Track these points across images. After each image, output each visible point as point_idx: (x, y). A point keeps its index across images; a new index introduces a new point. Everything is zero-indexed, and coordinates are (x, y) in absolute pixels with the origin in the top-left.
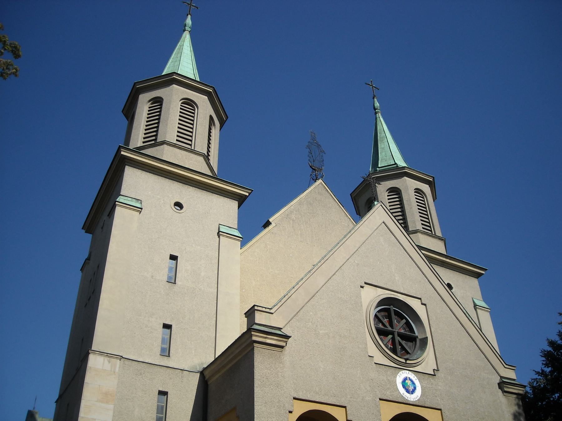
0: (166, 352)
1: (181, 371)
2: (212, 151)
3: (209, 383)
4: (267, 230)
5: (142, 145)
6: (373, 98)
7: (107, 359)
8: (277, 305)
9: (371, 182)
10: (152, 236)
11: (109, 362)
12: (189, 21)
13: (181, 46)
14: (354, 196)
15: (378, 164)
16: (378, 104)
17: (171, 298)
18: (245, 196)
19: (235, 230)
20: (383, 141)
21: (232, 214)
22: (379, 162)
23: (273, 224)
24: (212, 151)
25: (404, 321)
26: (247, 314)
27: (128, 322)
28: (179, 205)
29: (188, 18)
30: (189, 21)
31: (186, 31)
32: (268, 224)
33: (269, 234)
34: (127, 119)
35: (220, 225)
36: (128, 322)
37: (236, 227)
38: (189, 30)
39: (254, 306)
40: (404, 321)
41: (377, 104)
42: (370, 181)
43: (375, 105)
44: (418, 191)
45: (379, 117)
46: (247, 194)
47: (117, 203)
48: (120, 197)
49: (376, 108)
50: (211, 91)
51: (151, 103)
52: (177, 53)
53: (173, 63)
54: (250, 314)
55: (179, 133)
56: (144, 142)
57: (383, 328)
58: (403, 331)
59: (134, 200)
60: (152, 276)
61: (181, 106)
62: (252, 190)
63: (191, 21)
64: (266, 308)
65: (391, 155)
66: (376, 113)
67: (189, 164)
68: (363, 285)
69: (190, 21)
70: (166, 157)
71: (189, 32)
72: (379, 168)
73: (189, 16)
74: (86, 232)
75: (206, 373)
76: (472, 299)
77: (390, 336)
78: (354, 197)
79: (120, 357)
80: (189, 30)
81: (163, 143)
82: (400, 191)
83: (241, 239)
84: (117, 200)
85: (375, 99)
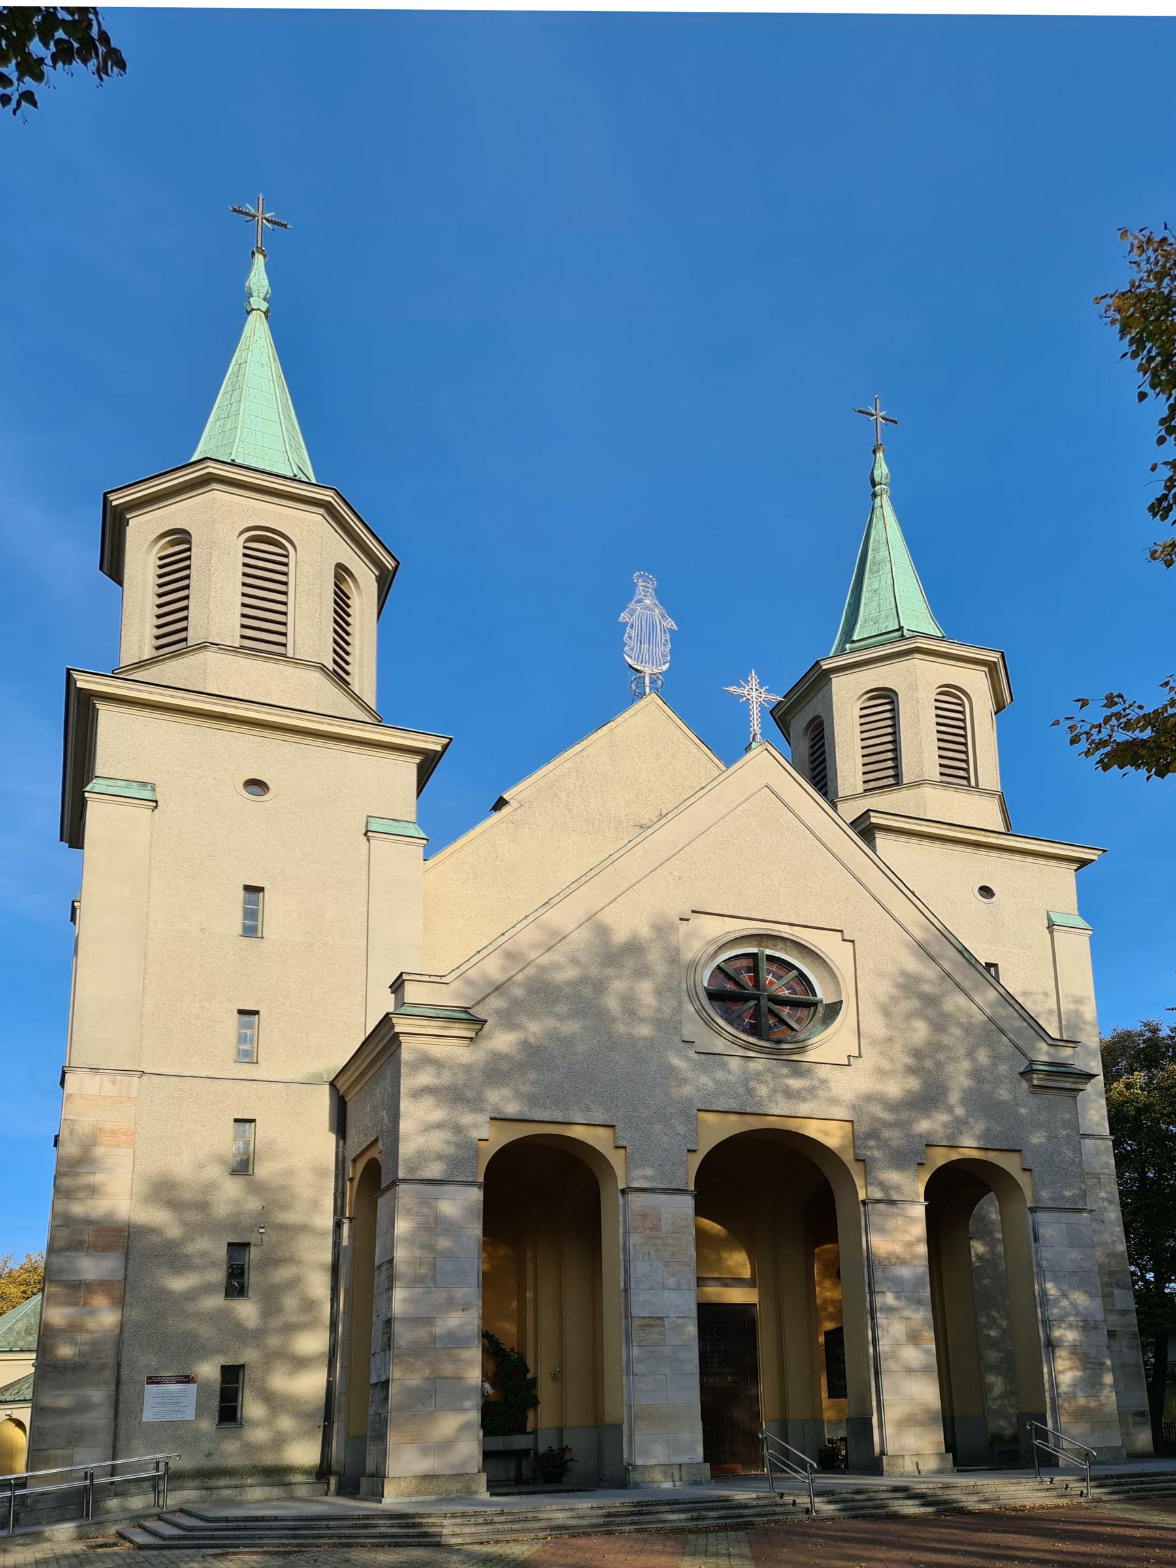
0: (247, 1056)
1: (284, 1085)
2: (357, 651)
3: (347, 1099)
4: (497, 816)
5: (156, 653)
6: (874, 452)
7: (106, 1078)
8: (458, 968)
9: (752, 697)
10: (193, 854)
11: (114, 1083)
12: (258, 279)
13: (240, 364)
14: (778, 715)
15: (851, 636)
16: (884, 466)
17: (254, 965)
18: (433, 754)
19: (412, 825)
20: (877, 571)
21: (401, 793)
22: (858, 626)
23: (513, 804)
24: (357, 651)
25: (795, 973)
26: (395, 987)
27: (153, 1014)
28: (256, 785)
29: (255, 266)
30: (258, 279)
31: (254, 312)
32: (500, 804)
33: (503, 825)
34: (117, 583)
35: (369, 819)
36: (153, 1014)
37: (413, 818)
38: (264, 306)
39: (401, 974)
40: (795, 973)
41: (882, 470)
42: (749, 697)
43: (876, 473)
44: (951, 693)
45: (882, 507)
46: (439, 748)
47: (86, 795)
48: (94, 781)
49: (877, 479)
50: (330, 499)
51: (169, 541)
52: (230, 389)
53: (219, 423)
54: (397, 986)
55: (161, 650)
56: (158, 648)
57: (734, 992)
58: (786, 992)
59: (135, 784)
60: (202, 930)
61: (245, 547)
62: (451, 739)
63: (266, 277)
64: (430, 976)
65: (894, 606)
66: (874, 495)
67: (280, 690)
68: (688, 915)
69: (264, 275)
70: (214, 680)
71: (266, 313)
72: (854, 642)
73: (259, 260)
74: (70, 847)
75: (342, 1085)
76: (1046, 913)
77: (752, 1003)
78: (779, 717)
79: (139, 1073)
80: (264, 306)
81: (202, 647)
82: (896, 694)
83: (425, 842)
84: (86, 789)
85: (878, 455)
